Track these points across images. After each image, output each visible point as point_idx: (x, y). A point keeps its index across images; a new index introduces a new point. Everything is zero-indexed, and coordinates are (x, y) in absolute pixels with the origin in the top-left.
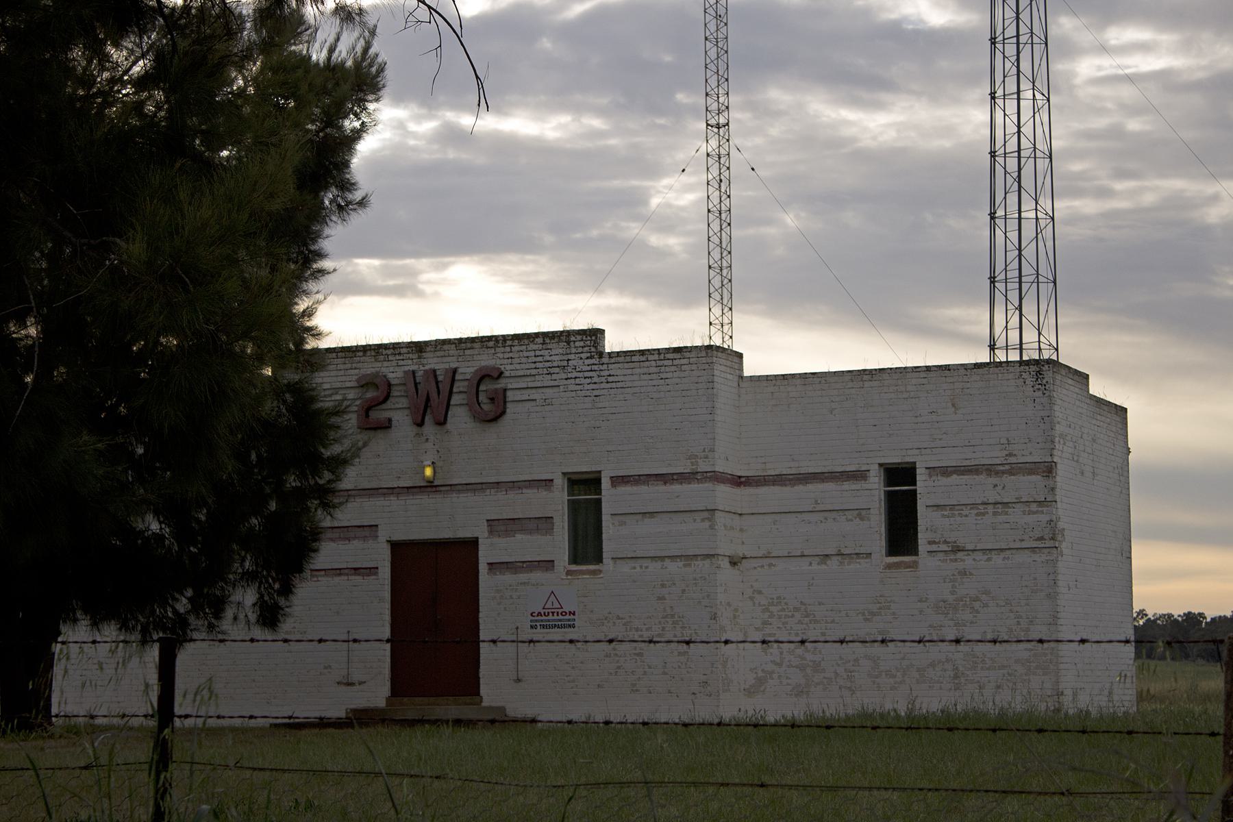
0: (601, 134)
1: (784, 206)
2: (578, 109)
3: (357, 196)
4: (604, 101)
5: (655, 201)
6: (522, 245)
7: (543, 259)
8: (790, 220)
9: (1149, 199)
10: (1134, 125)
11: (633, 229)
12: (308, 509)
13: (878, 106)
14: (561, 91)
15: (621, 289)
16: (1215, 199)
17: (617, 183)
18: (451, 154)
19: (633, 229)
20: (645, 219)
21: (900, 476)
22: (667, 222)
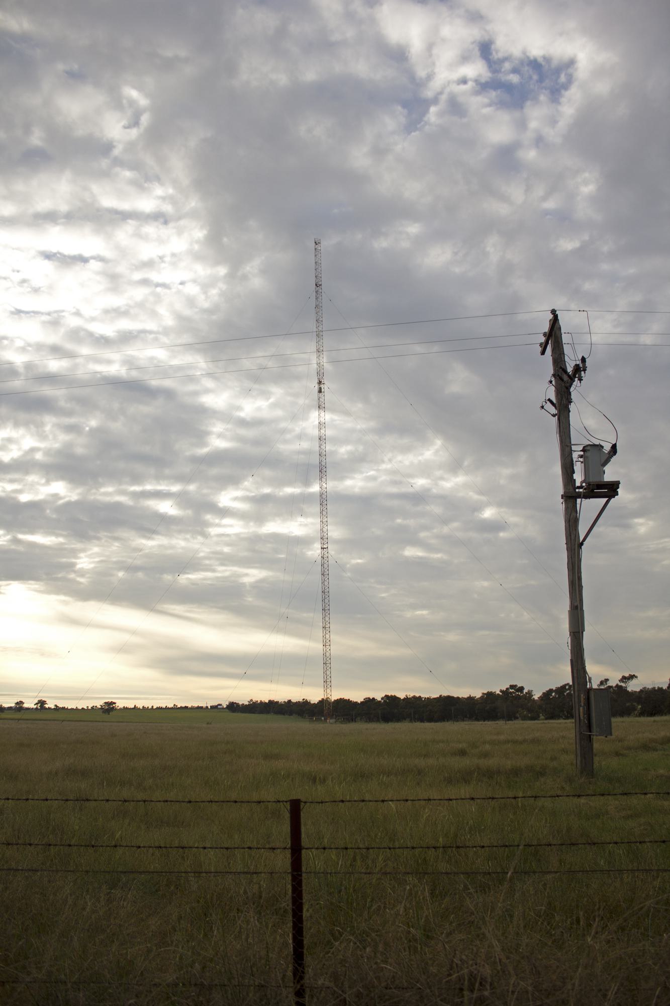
0: (62, 544)
1: (120, 569)
2: (57, 535)
3: (607, 447)
4: (65, 533)
5: (78, 566)
6: (36, 579)
7: (42, 583)
8: (121, 574)
9: (227, 574)
10: (226, 550)
11: (72, 576)
12: (217, 263)
13: (149, 538)
14: (50, 527)
15: (65, 594)
16: (247, 575)
17: (64, 560)
18: (13, 547)
19: (72, 576)
20: (75, 572)
21: (296, 807)
22: (82, 573)
